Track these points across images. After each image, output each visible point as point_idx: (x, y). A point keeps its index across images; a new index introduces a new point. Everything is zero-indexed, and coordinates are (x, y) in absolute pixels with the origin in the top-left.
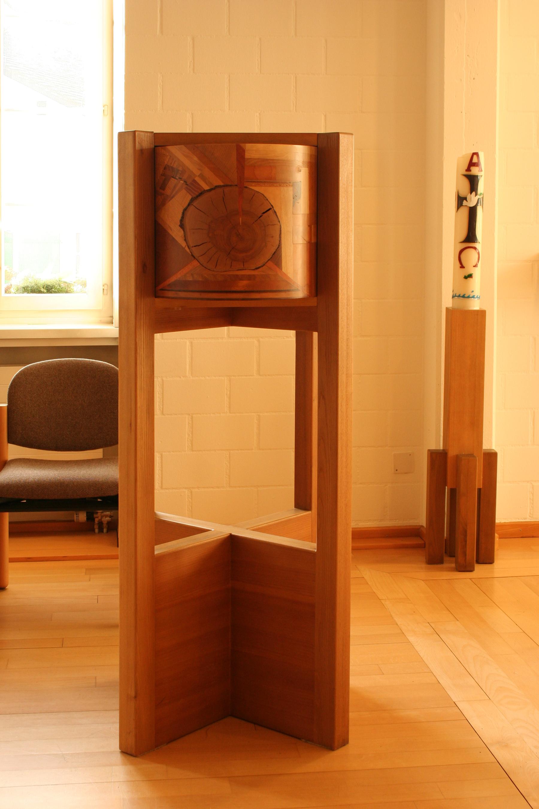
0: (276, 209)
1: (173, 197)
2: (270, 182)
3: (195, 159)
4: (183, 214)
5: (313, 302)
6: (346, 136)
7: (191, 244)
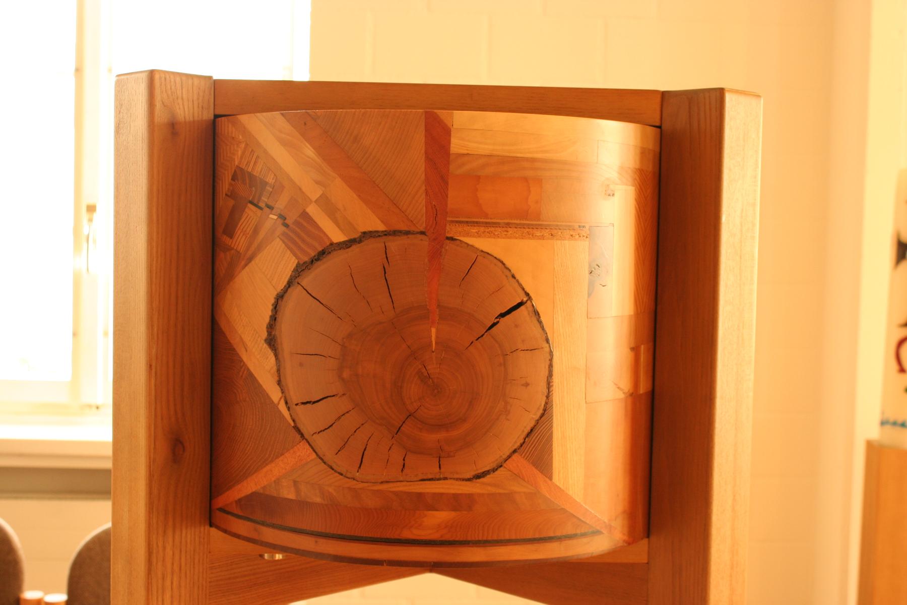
0: (539, 303)
1: (250, 260)
2: (523, 226)
3: (309, 151)
4: (276, 307)
5: (640, 553)
6: (743, 99)
7: (295, 398)
